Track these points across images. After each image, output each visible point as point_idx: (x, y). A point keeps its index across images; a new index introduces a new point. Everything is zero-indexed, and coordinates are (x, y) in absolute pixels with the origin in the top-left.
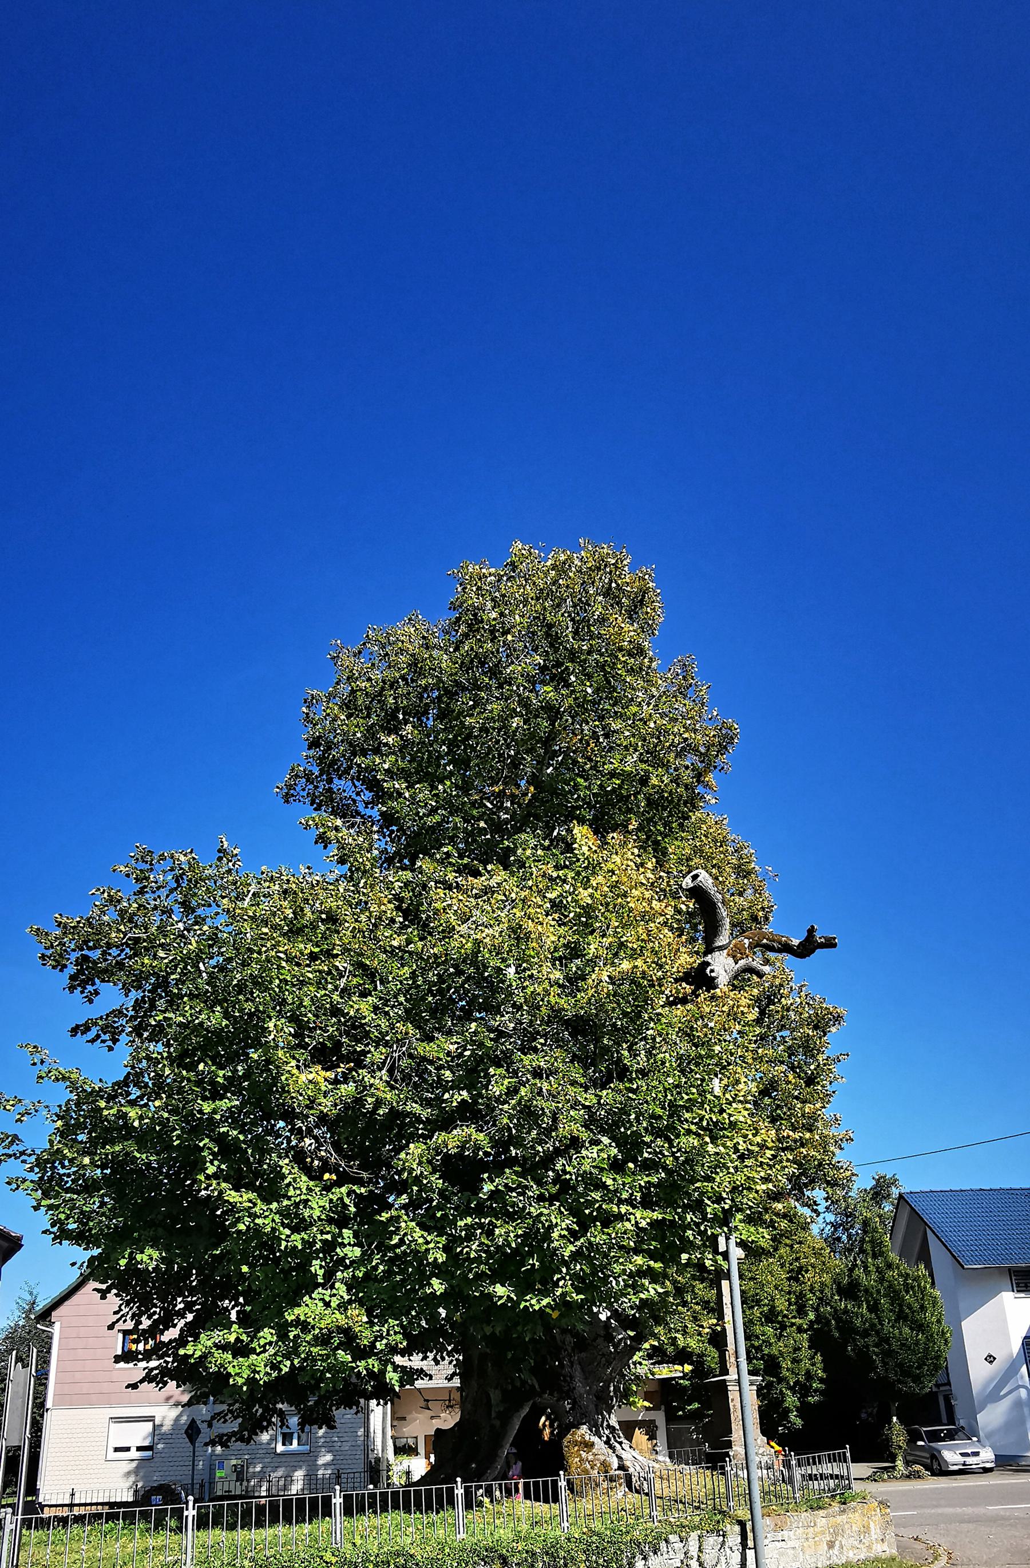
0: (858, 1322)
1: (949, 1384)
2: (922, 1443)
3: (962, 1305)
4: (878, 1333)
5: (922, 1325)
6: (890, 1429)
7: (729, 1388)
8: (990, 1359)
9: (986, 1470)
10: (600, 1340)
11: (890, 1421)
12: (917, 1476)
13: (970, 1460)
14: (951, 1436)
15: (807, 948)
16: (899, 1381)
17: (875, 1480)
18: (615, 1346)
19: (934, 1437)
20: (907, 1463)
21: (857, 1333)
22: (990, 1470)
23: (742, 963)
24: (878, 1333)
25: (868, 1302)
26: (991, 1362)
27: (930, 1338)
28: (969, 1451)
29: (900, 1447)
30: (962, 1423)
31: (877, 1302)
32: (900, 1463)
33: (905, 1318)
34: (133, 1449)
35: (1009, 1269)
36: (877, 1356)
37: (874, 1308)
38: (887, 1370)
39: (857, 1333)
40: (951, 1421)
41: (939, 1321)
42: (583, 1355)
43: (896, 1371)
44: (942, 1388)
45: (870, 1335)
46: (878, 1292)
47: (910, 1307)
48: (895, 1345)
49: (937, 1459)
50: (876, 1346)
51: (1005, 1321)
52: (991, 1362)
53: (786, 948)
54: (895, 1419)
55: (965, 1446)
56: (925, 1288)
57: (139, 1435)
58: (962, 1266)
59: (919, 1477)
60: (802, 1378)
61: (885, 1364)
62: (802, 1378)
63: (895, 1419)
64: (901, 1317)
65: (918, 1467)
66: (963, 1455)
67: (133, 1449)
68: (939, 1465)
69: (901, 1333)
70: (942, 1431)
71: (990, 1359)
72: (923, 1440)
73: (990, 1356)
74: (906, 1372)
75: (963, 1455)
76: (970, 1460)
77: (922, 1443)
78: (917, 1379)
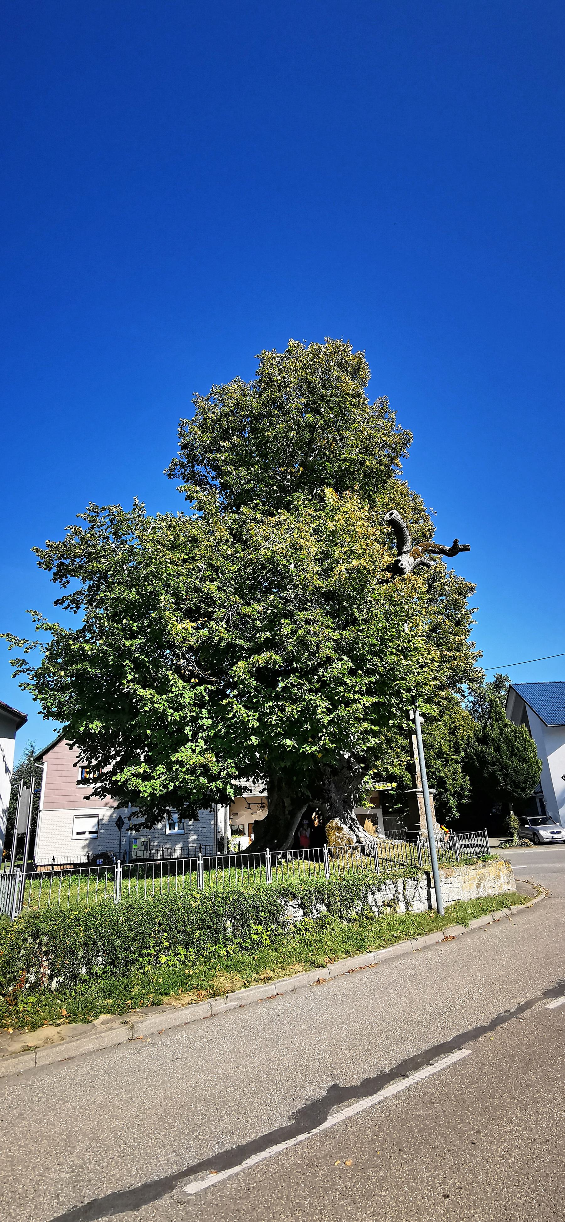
1: (542, 792)
3: (547, 747)
4: (500, 763)
5: (525, 759)
11: (509, 814)
13: (556, 836)
14: (544, 822)
19: (535, 822)
20: (520, 838)
21: (489, 764)
25: (494, 746)
27: (530, 766)
29: (515, 829)
31: (499, 746)
32: (515, 837)
33: (516, 755)
34: (87, 833)
37: (498, 749)
40: (544, 813)
41: (534, 757)
46: (500, 740)
47: (518, 748)
48: (510, 771)
50: (500, 771)
54: (512, 812)
61: (505, 781)
62: (459, 790)
63: (512, 812)
64: (513, 754)
65: (526, 840)
66: (552, 833)
67: (87, 833)
74: (517, 785)
75: (552, 833)
76: (556, 836)
78: (524, 789)
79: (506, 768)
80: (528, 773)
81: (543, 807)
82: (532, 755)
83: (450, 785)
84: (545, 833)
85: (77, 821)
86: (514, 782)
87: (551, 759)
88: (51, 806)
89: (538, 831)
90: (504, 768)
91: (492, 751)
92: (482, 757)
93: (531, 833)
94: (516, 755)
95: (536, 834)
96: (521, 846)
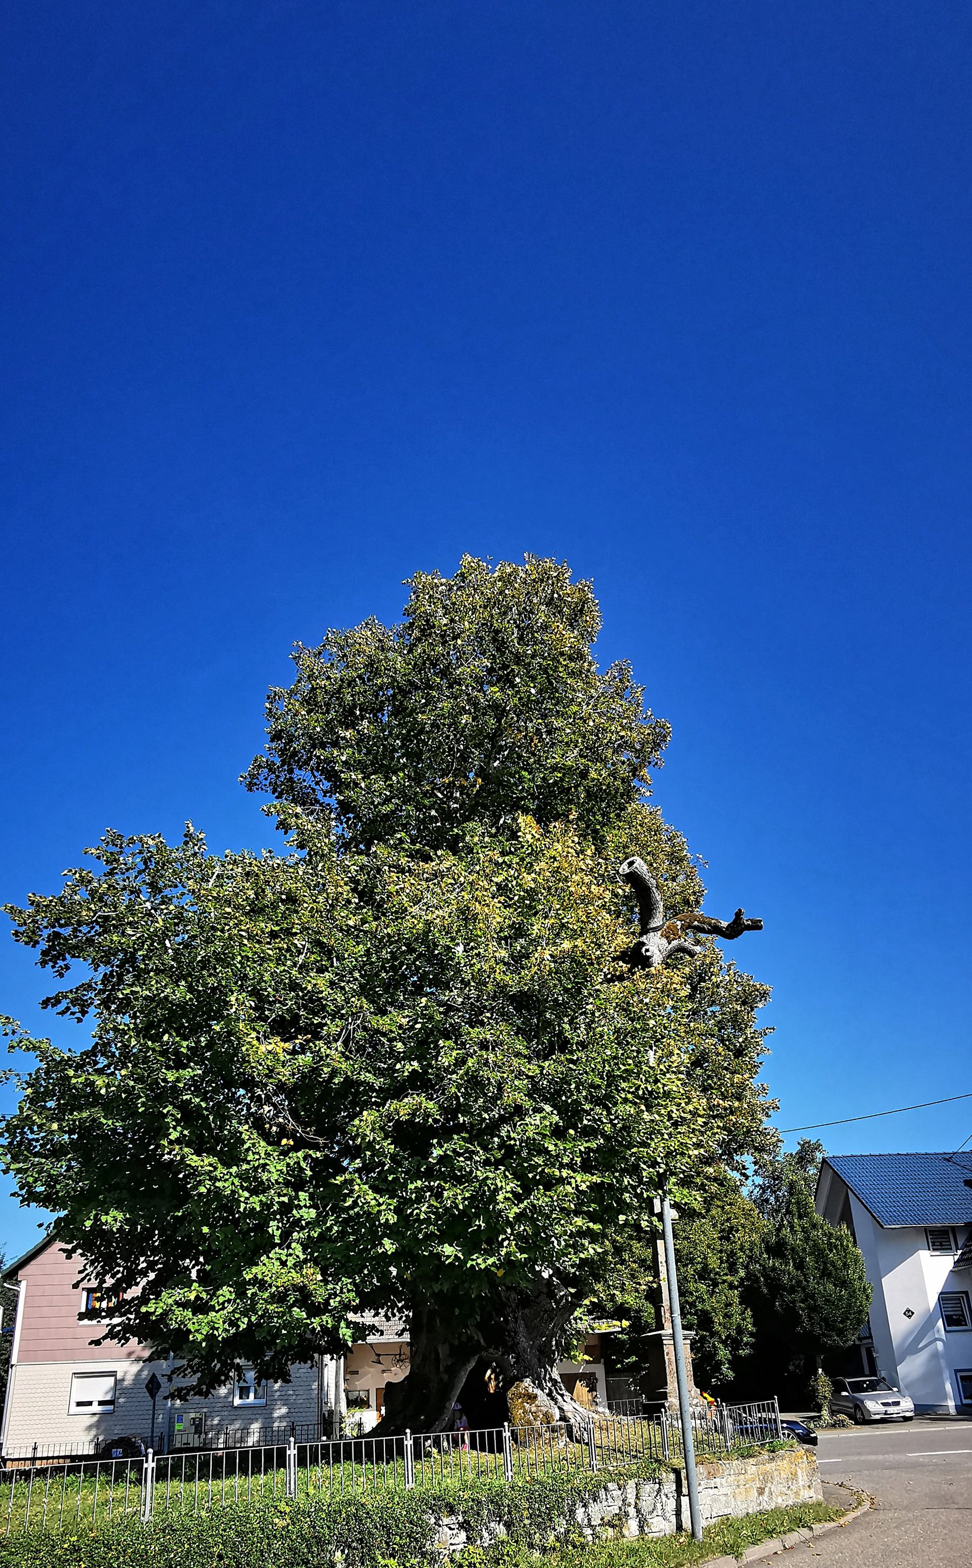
0: (785, 1279)
1: (871, 1337)
3: (881, 1263)
4: (804, 1289)
6: (816, 1380)
7: (665, 1342)
8: (909, 1313)
10: (543, 1297)
11: (816, 1373)
12: (842, 1425)
14: (873, 1386)
15: (735, 930)
16: (824, 1335)
18: (557, 1303)
19: (857, 1387)
21: (785, 1289)
23: (675, 943)
24: (804, 1289)
25: (794, 1260)
26: (909, 1317)
27: (852, 1295)
28: (890, 1401)
29: (825, 1398)
31: (802, 1261)
32: (825, 1413)
34: (95, 1404)
36: (803, 1311)
37: (800, 1266)
40: (873, 1372)
41: (860, 1278)
42: (526, 1311)
44: (864, 1342)
46: (804, 1250)
47: (833, 1264)
49: (860, 1409)
50: (803, 1301)
52: (909, 1317)
53: (716, 930)
54: (820, 1371)
55: (886, 1396)
58: (882, 1227)
59: (844, 1426)
61: (810, 1318)
63: (820, 1371)
65: (842, 1417)
66: (884, 1404)
67: (95, 1404)
68: (862, 1414)
71: (909, 1313)
73: (909, 1311)
74: (829, 1325)
75: (884, 1404)
76: (891, 1410)
78: (841, 1333)
80: (849, 1306)
81: (872, 1361)
82: (856, 1276)
84: (874, 1406)
86: (825, 1320)
96: (833, 1426)
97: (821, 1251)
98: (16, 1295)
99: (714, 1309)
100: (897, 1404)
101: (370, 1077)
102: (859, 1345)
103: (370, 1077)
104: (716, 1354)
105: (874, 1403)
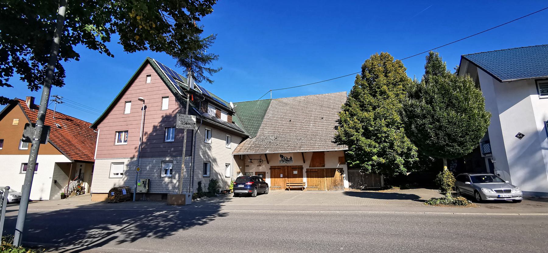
0: (418, 111)
1: (491, 153)
2: (469, 183)
3: (499, 107)
4: (433, 117)
5: (466, 109)
6: (442, 174)
9: (515, 201)
11: (442, 169)
12: (461, 204)
13: (503, 195)
14: (490, 179)
16: (447, 145)
17: (431, 204)
19: (479, 180)
20: (454, 195)
21: (418, 117)
22: (519, 201)
24: (433, 117)
25: (426, 98)
26: (520, 138)
27: (471, 117)
28: (503, 189)
29: (449, 185)
30: (498, 172)
31: (432, 98)
32: (449, 195)
33: (453, 106)
34: (119, 174)
35: (536, 80)
36: (431, 129)
37: (430, 102)
38: (438, 138)
39: (418, 117)
40: (492, 172)
41: (480, 109)
43: (445, 139)
44: (487, 155)
45: (426, 117)
46: (434, 92)
47: (457, 98)
48: (444, 123)
49: (478, 193)
50: (431, 124)
51: (532, 112)
52: (520, 138)
54: (446, 168)
55: (500, 186)
56: (469, 87)
57: (122, 169)
58: (500, 81)
59: (462, 204)
60: (405, 151)
61: (437, 135)
62: (405, 151)
63: (446, 168)
64: (450, 105)
65: (461, 198)
66: (497, 191)
67: (119, 174)
68: (480, 196)
69: (448, 114)
70: (484, 176)
72: (469, 181)
74: (452, 138)
75: (497, 191)
76: (503, 195)
77: (469, 183)
78: (461, 144)
79: (438, 121)
80: (469, 126)
81: (492, 166)
82: (476, 105)
83: (398, 146)
84: (489, 192)
85: (113, 166)
86: (449, 135)
87: (504, 117)
88: (101, 157)
89: (480, 189)
90: (435, 120)
91: (423, 103)
92: (411, 112)
93: (472, 190)
94: (453, 106)
95: (478, 191)
96: (454, 203)
97: (447, 91)
98: (97, 134)
99: (395, 139)
100: (509, 191)
101: (432, 134)
102: (484, 158)
103: (432, 134)
104: (395, 160)
105: (490, 190)
